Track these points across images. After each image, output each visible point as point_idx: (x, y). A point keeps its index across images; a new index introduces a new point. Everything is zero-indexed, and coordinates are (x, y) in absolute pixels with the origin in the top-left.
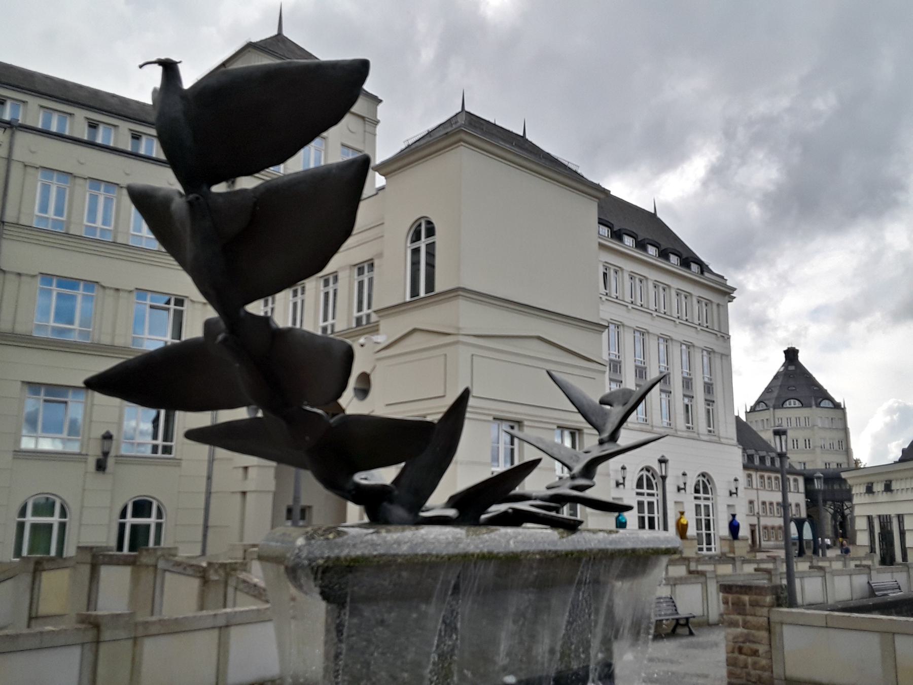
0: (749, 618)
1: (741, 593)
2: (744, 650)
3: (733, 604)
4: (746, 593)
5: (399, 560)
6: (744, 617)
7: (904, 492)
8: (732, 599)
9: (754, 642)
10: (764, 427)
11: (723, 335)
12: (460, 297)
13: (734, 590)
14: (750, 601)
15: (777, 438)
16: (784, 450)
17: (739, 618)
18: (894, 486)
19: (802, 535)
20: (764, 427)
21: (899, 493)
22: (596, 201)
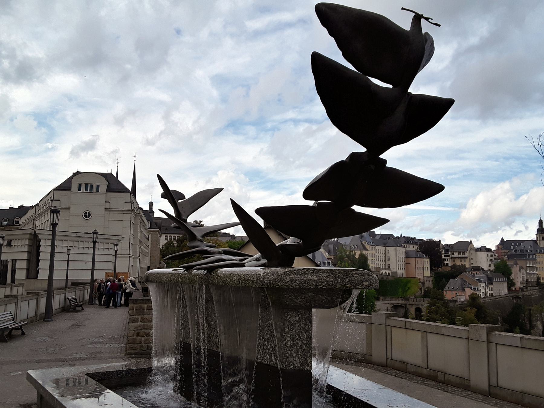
0: (145, 316)
1: (143, 304)
2: (141, 334)
3: (136, 310)
4: (146, 304)
5: (539, 281)
6: (142, 316)
7: (19, 247)
8: (137, 307)
9: (147, 329)
10: (496, 280)
11: (417, 268)
12: (5, 225)
13: (139, 302)
14: (147, 307)
15: (115, 246)
16: (117, 250)
17: (140, 317)
18: (13, 243)
19: (15, 276)
20: (496, 280)
21: (16, 247)
22: (504, 281)
